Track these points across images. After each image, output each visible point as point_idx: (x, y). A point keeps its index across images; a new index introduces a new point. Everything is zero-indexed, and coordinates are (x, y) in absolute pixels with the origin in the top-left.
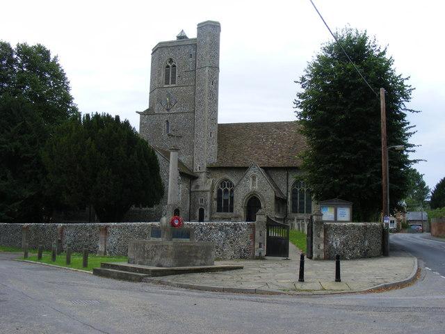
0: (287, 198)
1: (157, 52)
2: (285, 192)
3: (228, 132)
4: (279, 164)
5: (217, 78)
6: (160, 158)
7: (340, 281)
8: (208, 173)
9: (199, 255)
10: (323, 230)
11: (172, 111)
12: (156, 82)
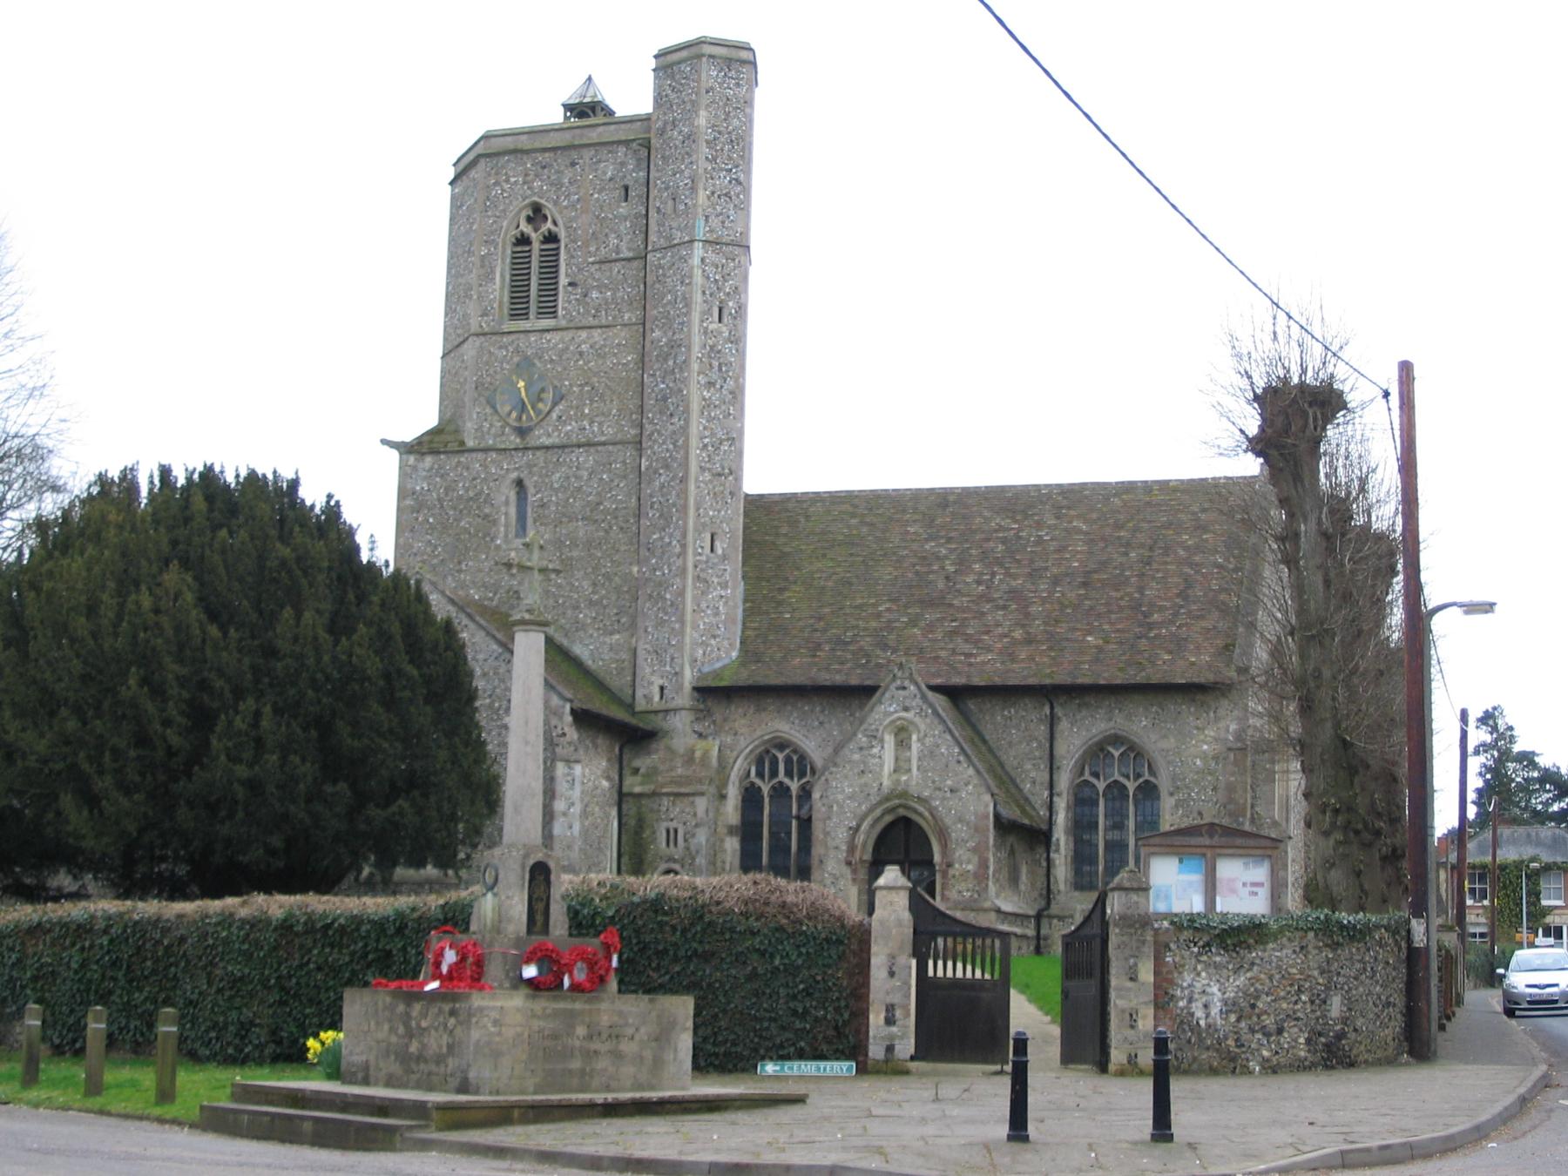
0: (1051, 823)
1: (473, 173)
2: (1040, 797)
3: (781, 533)
4: (1020, 673)
5: (739, 291)
6: (472, 637)
7: (1169, 1138)
8: (701, 714)
9: (628, 1047)
10: (1149, 950)
11: (540, 437)
12: (472, 309)
